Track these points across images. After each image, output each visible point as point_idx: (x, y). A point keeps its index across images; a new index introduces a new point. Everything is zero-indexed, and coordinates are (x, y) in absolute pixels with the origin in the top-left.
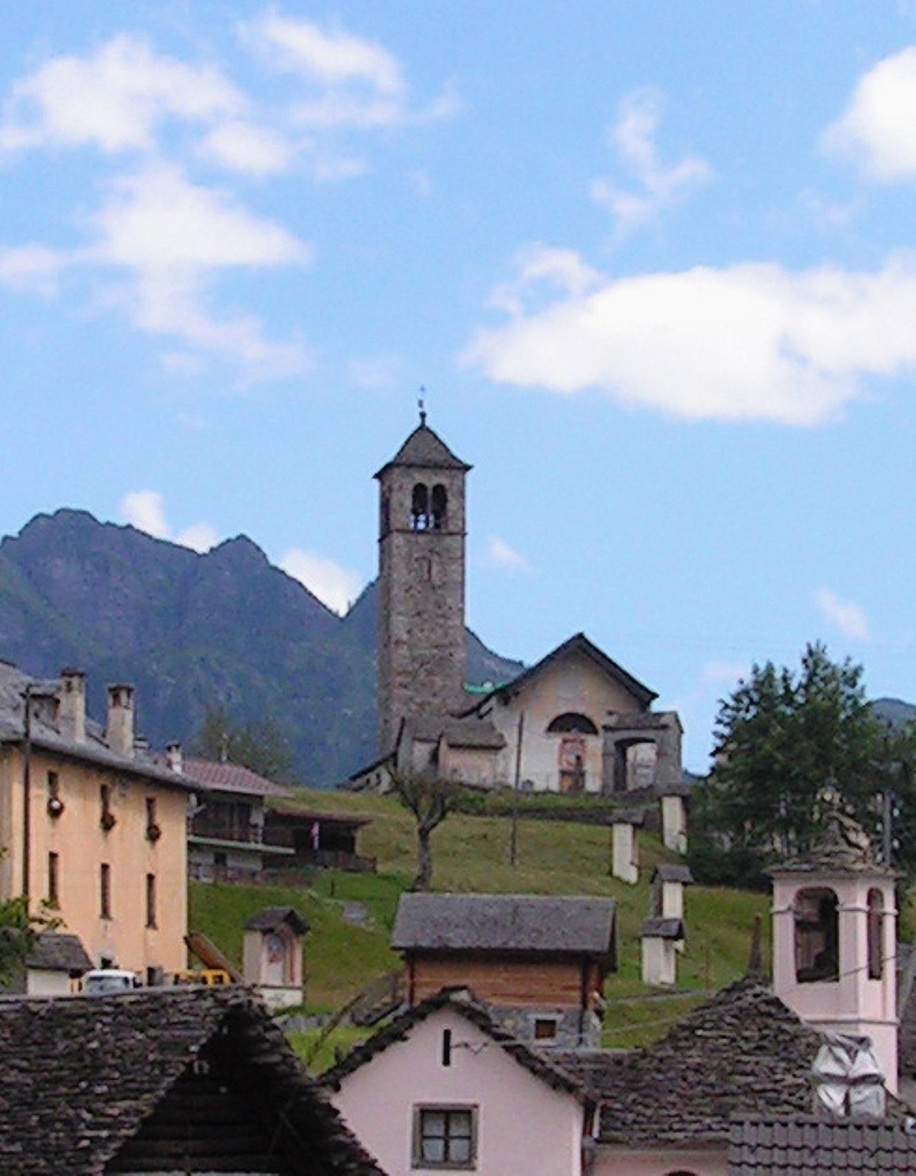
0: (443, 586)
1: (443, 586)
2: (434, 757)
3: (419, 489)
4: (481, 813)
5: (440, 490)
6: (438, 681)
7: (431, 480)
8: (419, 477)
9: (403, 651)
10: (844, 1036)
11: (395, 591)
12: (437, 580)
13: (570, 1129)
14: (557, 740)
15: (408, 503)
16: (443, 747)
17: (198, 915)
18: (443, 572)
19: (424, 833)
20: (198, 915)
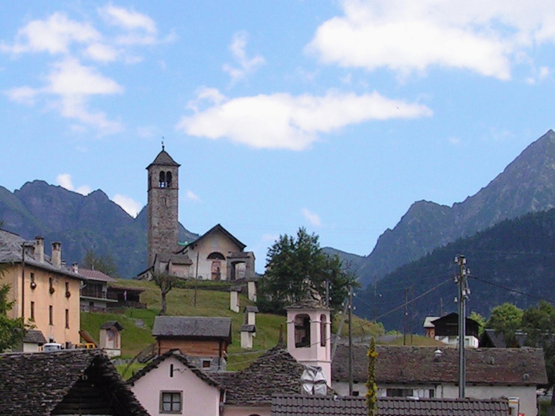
0: (170, 207)
1: (170, 207)
2: (167, 268)
3: (162, 173)
4: (184, 288)
6: (169, 241)
7: (166, 170)
8: (162, 169)
9: (156, 230)
12: (168, 205)
14: (210, 262)
15: (158, 178)
18: (171, 202)
19: (164, 295)
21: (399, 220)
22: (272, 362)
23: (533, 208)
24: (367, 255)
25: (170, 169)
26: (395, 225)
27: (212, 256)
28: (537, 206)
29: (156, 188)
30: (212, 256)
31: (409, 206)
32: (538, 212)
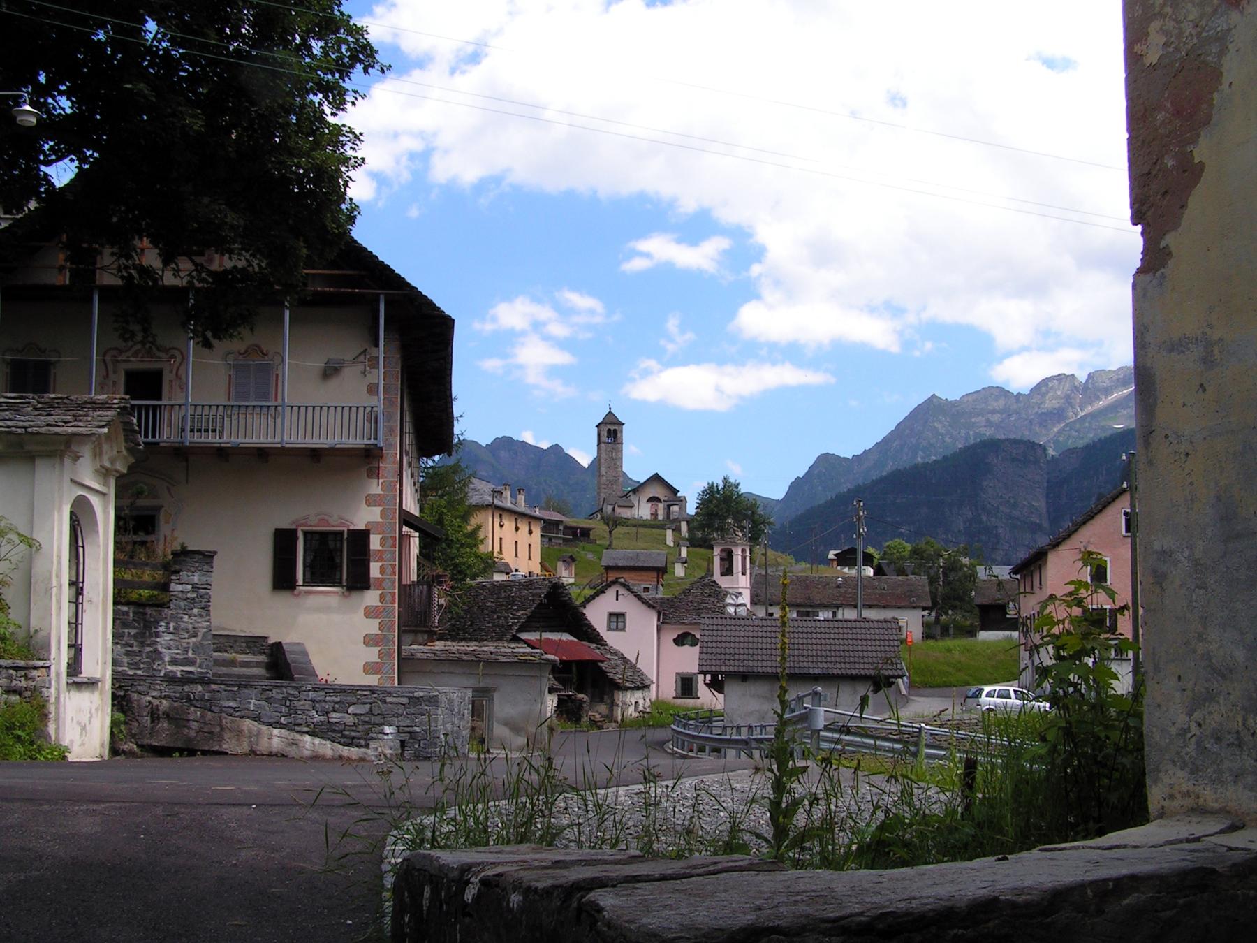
2: (614, 509)
3: (609, 430)
7: (612, 428)
8: (609, 427)
9: (604, 478)
14: (650, 504)
15: (606, 434)
19: (610, 532)
23: (919, 459)
26: (804, 473)
29: (604, 443)
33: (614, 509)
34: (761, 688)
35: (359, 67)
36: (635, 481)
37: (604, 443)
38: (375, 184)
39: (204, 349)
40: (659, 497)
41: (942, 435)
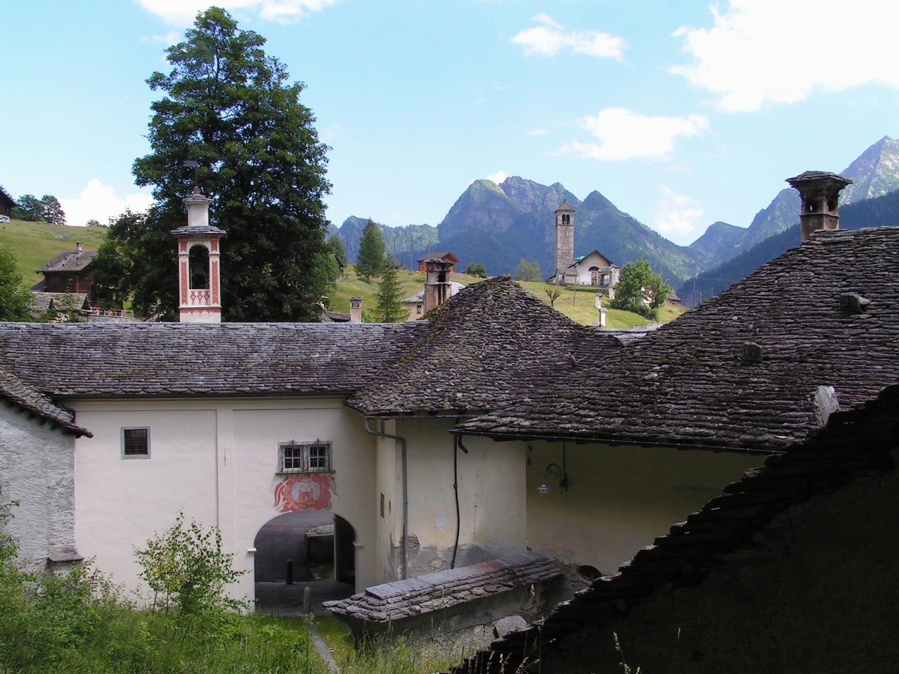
0: (569, 237)
1: (569, 237)
2: (563, 277)
3: (564, 216)
4: (572, 290)
5: (288, 465)
6: (568, 258)
7: (566, 214)
8: (564, 213)
9: (560, 251)
10: (419, 319)
11: (558, 238)
12: (567, 236)
13: (216, 244)
14: (591, 272)
15: (561, 219)
16: (565, 276)
17: (222, 272)
18: (569, 234)
19: (552, 301)
20: (222, 272)
21: (771, 203)
22: (516, 427)
23: (870, 193)
24: (747, 227)
25: (285, 470)
26: (767, 206)
27: (592, 269)
28: (873, 193)
29: (560, 225)
30: (592, 269)
31: (778, 193)
32: (873, 198)
33: (563, 277)
34: (519, 444)
35: (323, 193)
36: (623, 214)
37: (560, 225)
38: (338, 404)
39: (234, 18)
40: (596, 266)
41: (891, 171)
